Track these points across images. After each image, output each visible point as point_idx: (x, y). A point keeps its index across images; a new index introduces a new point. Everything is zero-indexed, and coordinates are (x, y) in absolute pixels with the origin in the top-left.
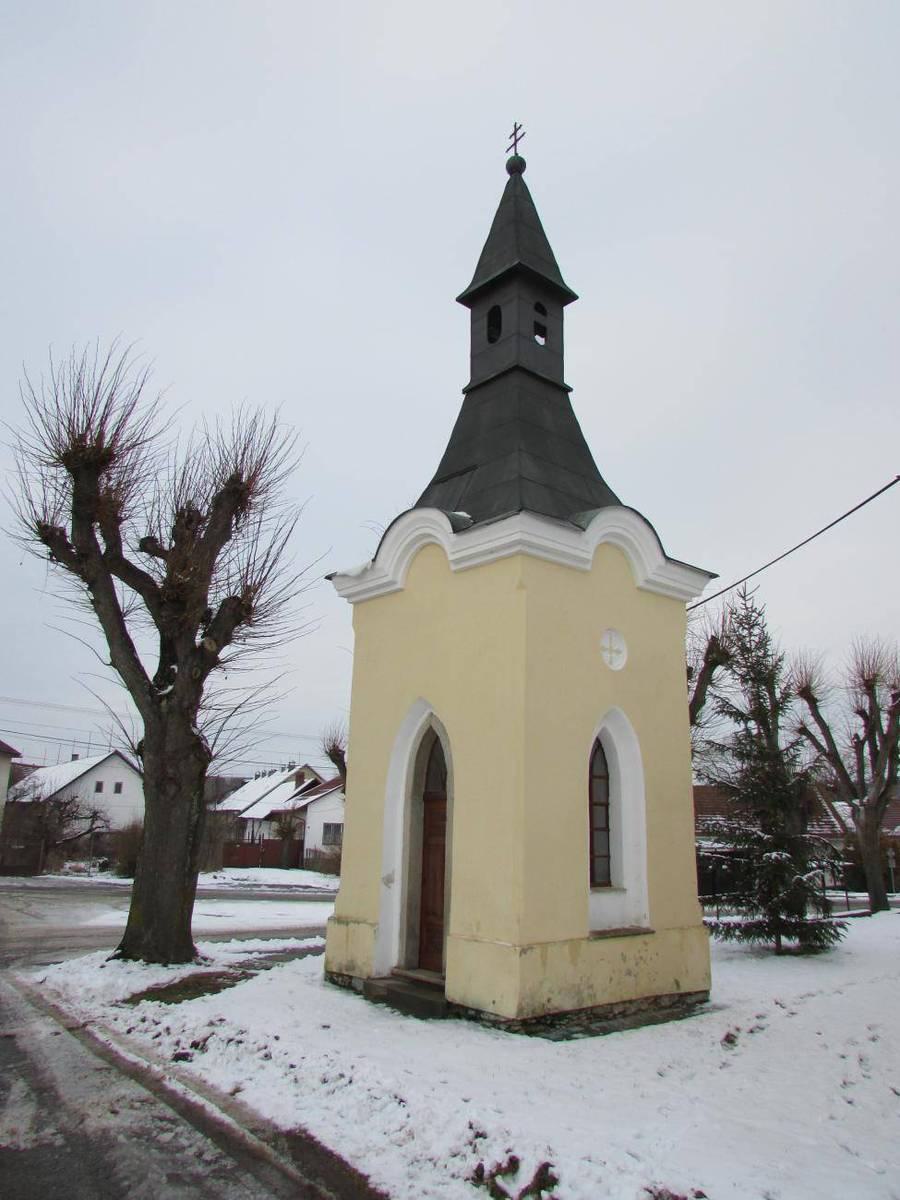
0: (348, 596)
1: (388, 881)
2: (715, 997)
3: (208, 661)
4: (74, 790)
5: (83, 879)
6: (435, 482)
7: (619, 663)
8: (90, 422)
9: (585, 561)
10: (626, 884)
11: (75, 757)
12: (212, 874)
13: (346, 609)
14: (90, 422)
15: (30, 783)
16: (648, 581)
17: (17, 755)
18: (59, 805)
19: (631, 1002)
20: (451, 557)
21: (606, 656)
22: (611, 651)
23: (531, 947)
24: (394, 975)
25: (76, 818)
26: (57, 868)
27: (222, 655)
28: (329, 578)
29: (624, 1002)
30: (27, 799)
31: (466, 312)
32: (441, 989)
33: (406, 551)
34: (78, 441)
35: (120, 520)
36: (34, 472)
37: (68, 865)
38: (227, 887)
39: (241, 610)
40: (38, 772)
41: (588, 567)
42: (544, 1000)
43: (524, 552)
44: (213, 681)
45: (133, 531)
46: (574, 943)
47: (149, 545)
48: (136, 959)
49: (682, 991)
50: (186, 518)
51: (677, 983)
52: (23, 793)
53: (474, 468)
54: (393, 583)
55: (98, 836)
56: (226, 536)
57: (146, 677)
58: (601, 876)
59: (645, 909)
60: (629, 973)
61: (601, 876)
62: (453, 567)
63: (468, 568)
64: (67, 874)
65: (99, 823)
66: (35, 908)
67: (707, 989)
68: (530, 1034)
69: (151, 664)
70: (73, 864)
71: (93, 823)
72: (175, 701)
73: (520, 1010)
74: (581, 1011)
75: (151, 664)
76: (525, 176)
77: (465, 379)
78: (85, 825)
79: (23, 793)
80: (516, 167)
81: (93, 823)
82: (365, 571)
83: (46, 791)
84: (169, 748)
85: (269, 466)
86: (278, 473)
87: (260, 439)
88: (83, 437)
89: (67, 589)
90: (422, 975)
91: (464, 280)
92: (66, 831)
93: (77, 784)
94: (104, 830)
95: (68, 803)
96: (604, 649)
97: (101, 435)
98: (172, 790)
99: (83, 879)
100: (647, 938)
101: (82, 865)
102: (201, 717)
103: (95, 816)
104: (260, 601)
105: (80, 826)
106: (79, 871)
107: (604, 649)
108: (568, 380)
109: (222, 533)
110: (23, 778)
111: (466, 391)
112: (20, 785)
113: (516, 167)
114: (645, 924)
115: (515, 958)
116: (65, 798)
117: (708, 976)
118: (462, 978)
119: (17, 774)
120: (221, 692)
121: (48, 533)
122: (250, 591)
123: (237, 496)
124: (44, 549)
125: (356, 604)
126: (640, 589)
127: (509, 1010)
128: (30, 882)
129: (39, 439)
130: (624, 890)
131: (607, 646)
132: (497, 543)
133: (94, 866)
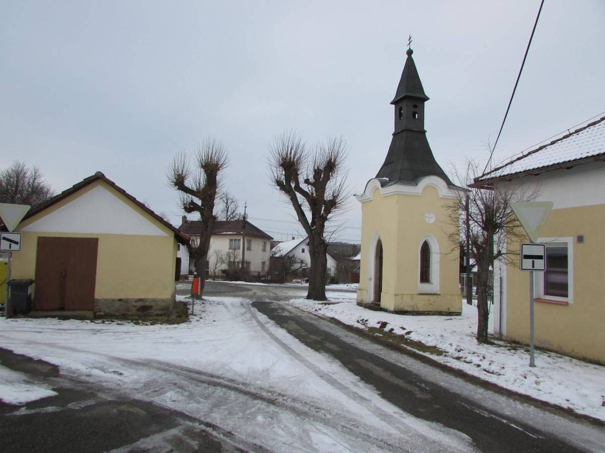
0: (360, 201)
1: (370, 279)
2: (462, 314)
3: (325, 219)
4: (294, 252)
5: (300, 285)
6: (385, 165)
7: (432, 221)
8: (287, 154)
9: (419, 193)
10: (433, 282)
11: (293, 238)
12: (346, 285)
13: (360, 204)
14: (287, 154)
15: (278, 249)
16: (443, 196)
17: (272, 239)
18: (289, 258)
19: (431, 311)
20: (382, 193)
21: (427, 220)
22: (429, 217)
23: (398, 295)
24: (372, 303)
25: (295, 263)
26: (291, 281)
27: (328, 217)
28: (354, 195)
29: (428, 311)
30: (277, 255)
31: (393, 106)
32: (379, 305)
33: (373, 189)
34: (284, 159)
35: (298, 175)
36: (274, 169)
37: (294, 281)
38: (351, 289)
39: (332, 204)
40: (280, 245)
41: (420, 195)
42: (402, 307)
43: (399, 194)
44: (326, 224)
45: (301, 179)
46: (412, 295)
47: (307, 181)
48: (311, 299)
49: (450, 311)
50: (317, 172)
51: (449, 309)
52: (275, 253)
53: (393, 162)
54: (369, 198)
55: (304, 270)
56: (328, 179)
57: (308, 222)
58: (425, 277)
59: (438, 289)
60: (431, 304)
61: (425, 277)
62: (383, 196)
63: (386, 196)
64: (294, 283)
65: (303, 265)
66: (284, 291)
67: (460, 312)
68: (397, 314)
69: (310, 220)
70: (296, 280)
71: (301, 264)
72: (316, 231)
73: (395, 309)
74: (414, 311)
75: (310, 220)
76: (412, 56)
77: (393, 131)
78: (299, 265)
79: (275, 253)
80: (410, 52)
81: (301, 264)
82: (362, 195)
83: (284, 253)
84: (316, 244)
85: (340, 155)
86: (343, 157)
87: (338, 142)
88: (286, 159)
89: (284, 198)
90: (377, 303)
91: (392, 96)
92: (292, 268)
93: (295, 250)
94: (306, 267)
95: (292, 258)
96: (426, 217)
97: (290, 158)
98: (317, 255)
99: (300, 285)
100: (438, 296)
101: (299, 280)
102: (325, 235)
103: (302, 262)
104: (338, 200)
105: (297, 266)
106: (298, 282)
107: (426, 217)
108: (425, 129)
109: (327, 178)
110: (275, 247)
111: (394, 135)
112: (274, 250)
113: (410, 52)
114: (438, 293)
115: (394, 297)
116: (291, 255)
117: (462, 309)
118: (384, 303)
119: (274, 244)
120: (328, 227)
121: (279, 183)
122: (335, 197)
123: (224, 418)
124: (278, 187)
125: (362, 203)
126: (441, 198)
127: (392, 309)
128: (282, 285)
129: (274, 161)
130: (432, 283)
131: (428, 216)
132: (391, 191)
133: (303, 281)
